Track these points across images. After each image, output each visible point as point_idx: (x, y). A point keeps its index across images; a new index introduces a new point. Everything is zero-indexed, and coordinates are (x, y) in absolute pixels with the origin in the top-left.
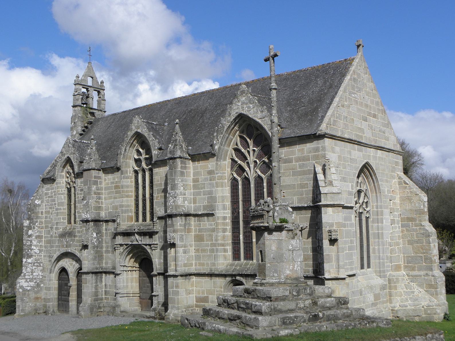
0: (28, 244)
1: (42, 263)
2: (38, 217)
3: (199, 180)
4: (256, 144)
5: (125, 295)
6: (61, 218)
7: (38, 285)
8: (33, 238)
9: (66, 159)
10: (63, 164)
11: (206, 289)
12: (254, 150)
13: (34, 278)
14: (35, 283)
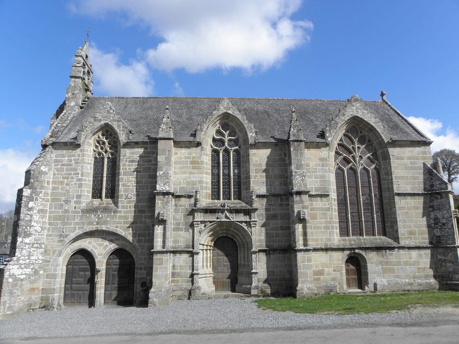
0: (26, 219)
1: (44, 243)
2: (42, 187)
3: (309, 165)
4: (361, 142)
5: (204, 276)
6: (85, 190)
7: (36, 272)
8: (35, 211)
9: (101, 125)
10: (95, 131)
11: (321, 263)
12: (359, 148)
13: (31, 263)
14: (32, 269)
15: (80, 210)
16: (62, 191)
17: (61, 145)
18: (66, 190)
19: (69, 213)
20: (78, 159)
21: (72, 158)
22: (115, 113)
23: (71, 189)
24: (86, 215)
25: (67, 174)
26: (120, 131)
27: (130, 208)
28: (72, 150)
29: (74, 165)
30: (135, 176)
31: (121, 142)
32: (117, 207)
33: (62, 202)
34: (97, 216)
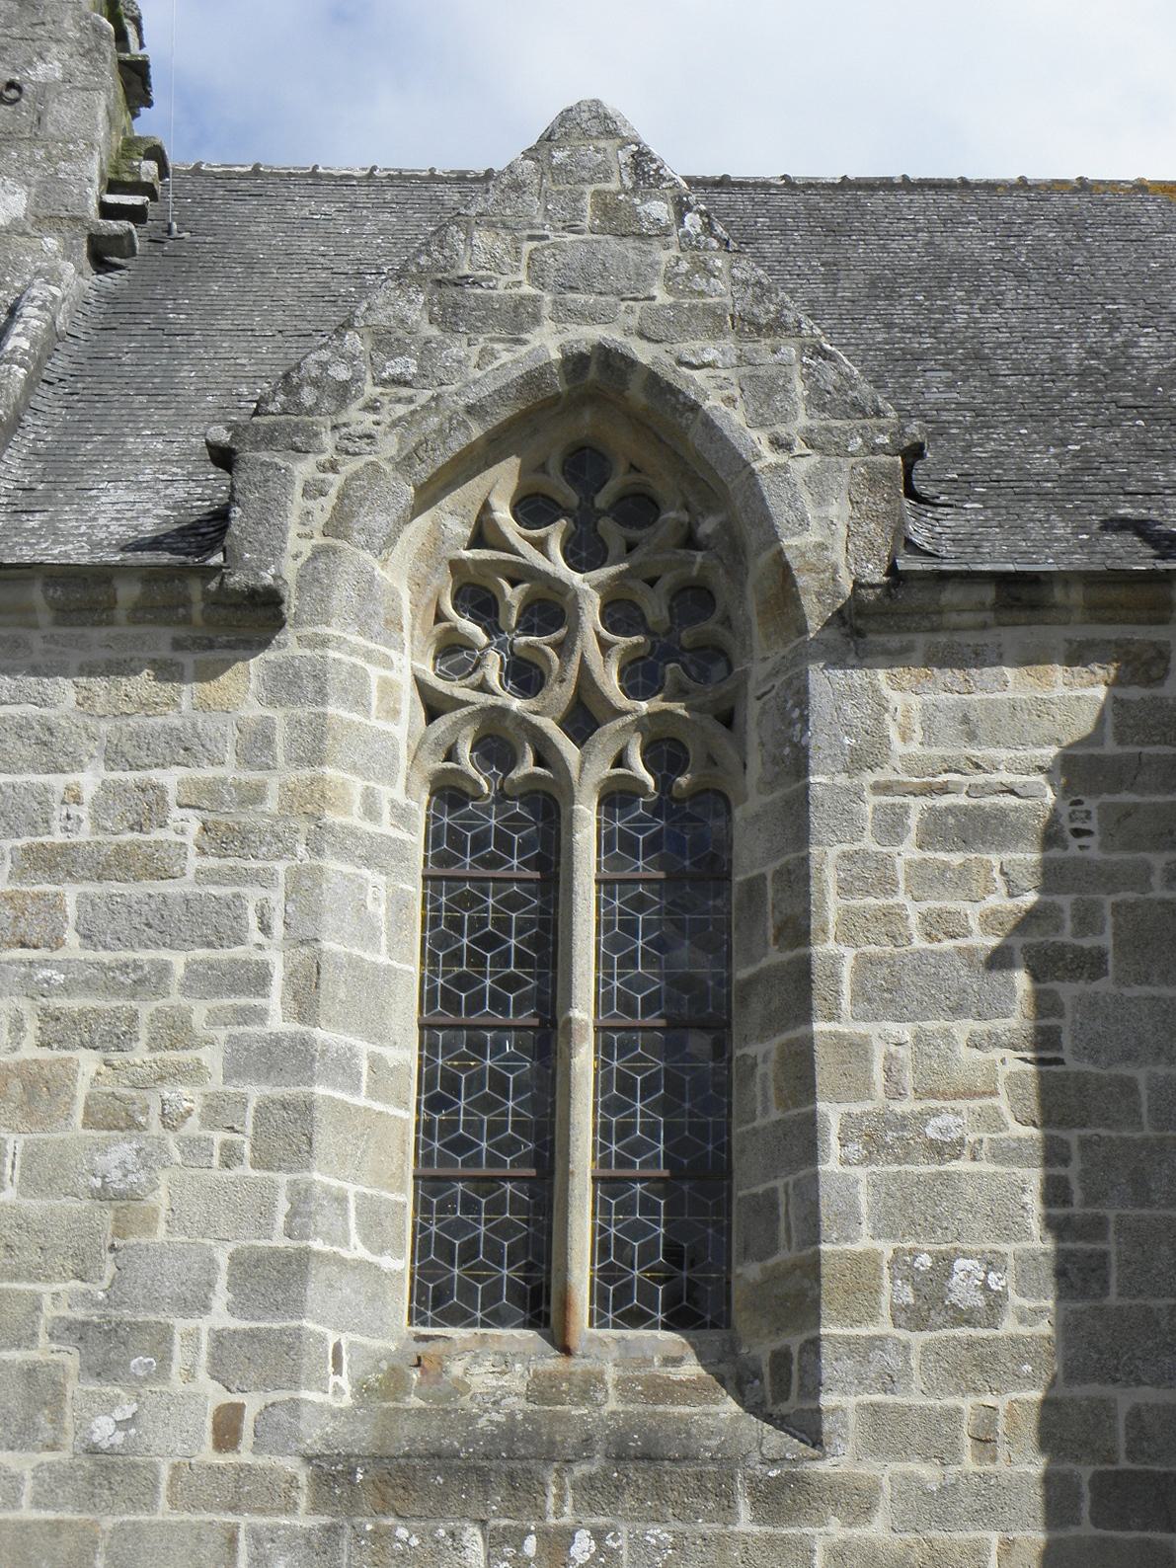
9: (533, 380)
10: (457, 443)
15: (291, 1465)
16: (35, 1206)
17: (24, 615)
18: (101, 1195)
19: (151, 1507)
20: (253, 795)
21: (170, 778)
22: (708, 228)
23: (163, 1178)
24: (382, 1536)
25: (103, 981)
26: (780, 444)
27: (984, 1441)
28: (167, 672)
29: (194, 862)
30: (1018, 1019)
31: (803, 580)
32: (810, 1430)
33: (43, 1351)
34: (531, 1545)
